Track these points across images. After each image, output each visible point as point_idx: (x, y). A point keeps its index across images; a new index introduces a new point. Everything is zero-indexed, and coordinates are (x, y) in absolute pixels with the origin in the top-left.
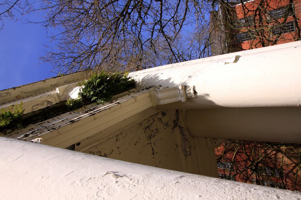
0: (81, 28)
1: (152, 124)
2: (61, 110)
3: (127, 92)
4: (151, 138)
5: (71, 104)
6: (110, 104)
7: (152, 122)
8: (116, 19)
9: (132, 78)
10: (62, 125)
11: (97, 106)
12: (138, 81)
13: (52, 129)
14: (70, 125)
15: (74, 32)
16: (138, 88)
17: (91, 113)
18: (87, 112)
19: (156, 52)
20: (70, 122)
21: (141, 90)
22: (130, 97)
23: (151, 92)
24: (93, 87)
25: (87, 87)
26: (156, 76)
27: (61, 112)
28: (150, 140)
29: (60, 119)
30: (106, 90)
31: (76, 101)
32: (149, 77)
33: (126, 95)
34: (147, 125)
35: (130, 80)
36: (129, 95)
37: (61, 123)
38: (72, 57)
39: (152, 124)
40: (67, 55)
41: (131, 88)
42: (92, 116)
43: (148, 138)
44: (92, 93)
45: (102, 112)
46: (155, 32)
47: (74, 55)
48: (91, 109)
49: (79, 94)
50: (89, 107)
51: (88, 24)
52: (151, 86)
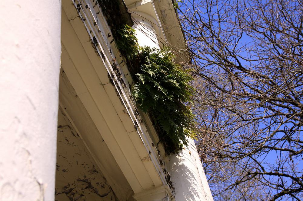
0: (269, 33)
1: (96, 192)
2: (115, 17)
3: (157, 139)
4: (67, 193)
5: (127, 36)
6: (134, 111)
7: (100, 193)
8: (293, 98)
9: (184, 146)
10: (87, 24)
11: (127, 86)
12: (180, 158)
13: (78, 5)
14: (88, 39)
15: (261, 20)
16: (167, 159)
17: (113, 76)
18: (114, 68)
19: (237, 183)
20: (94, 38)
21: (163, 167)
22: (150, 148)
23: (163, 187)
24: (162, 74)
25: (162, 63)
26: (194, 195)
27: (111, 16)
28: (63, 192)
29: (97, 17)
30: (160, 100)
31: (133, 43)
32: (191, 179)
33: (153, 139)
34: (93, 183)
35: (182, 142)
36: (153, 146)
37: (90, 21)
38: (211, 21)
39: (96, 192)
40: (214, 10)
41: (165, 147)
42: (109, 80)
43: (66, 187)
44: (151, 73)
45: (140, 139)
46: (277, 177)
47: (215, 24)
48: (120, 75)
49: (147, 48)
50: (124, 70)
51: (278, 46)
52: (174, 185)
